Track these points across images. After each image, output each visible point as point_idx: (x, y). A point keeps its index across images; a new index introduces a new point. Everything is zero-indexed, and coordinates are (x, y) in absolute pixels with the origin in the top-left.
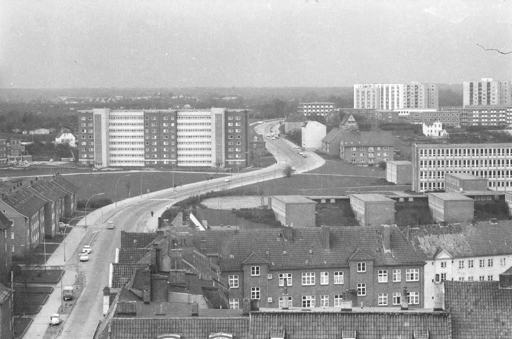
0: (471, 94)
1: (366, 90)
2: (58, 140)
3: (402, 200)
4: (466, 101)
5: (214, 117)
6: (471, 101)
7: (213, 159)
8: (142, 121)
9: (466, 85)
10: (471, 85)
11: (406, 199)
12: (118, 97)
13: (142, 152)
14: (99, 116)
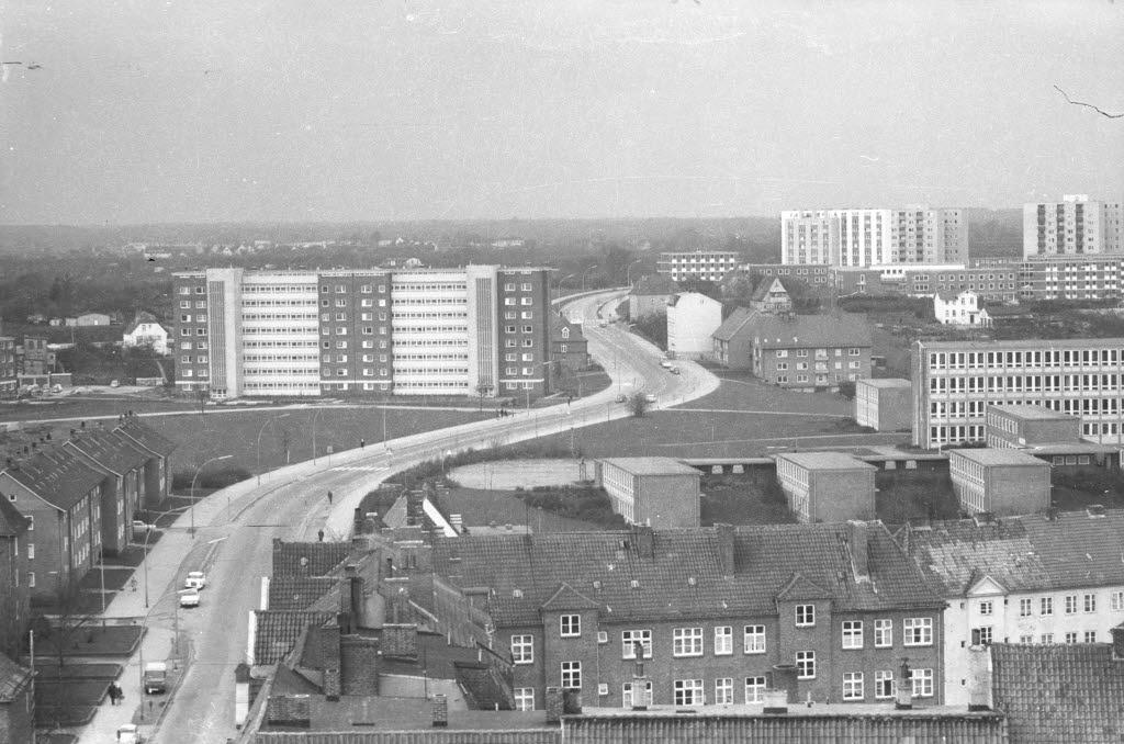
0: (1042, 231)
1: (808, 224)
2: (130, 339)
3: (890, 465)
4: (1030, 245)
5: (472, 285)
6: (1041, 246)
7: (473, 378)
8: (314, 296)
9: (1030, 211)
10: (1041, 210)
11: (900, 463)
12: (260, 244)
13: (316, 365)
14: (221, 285)
